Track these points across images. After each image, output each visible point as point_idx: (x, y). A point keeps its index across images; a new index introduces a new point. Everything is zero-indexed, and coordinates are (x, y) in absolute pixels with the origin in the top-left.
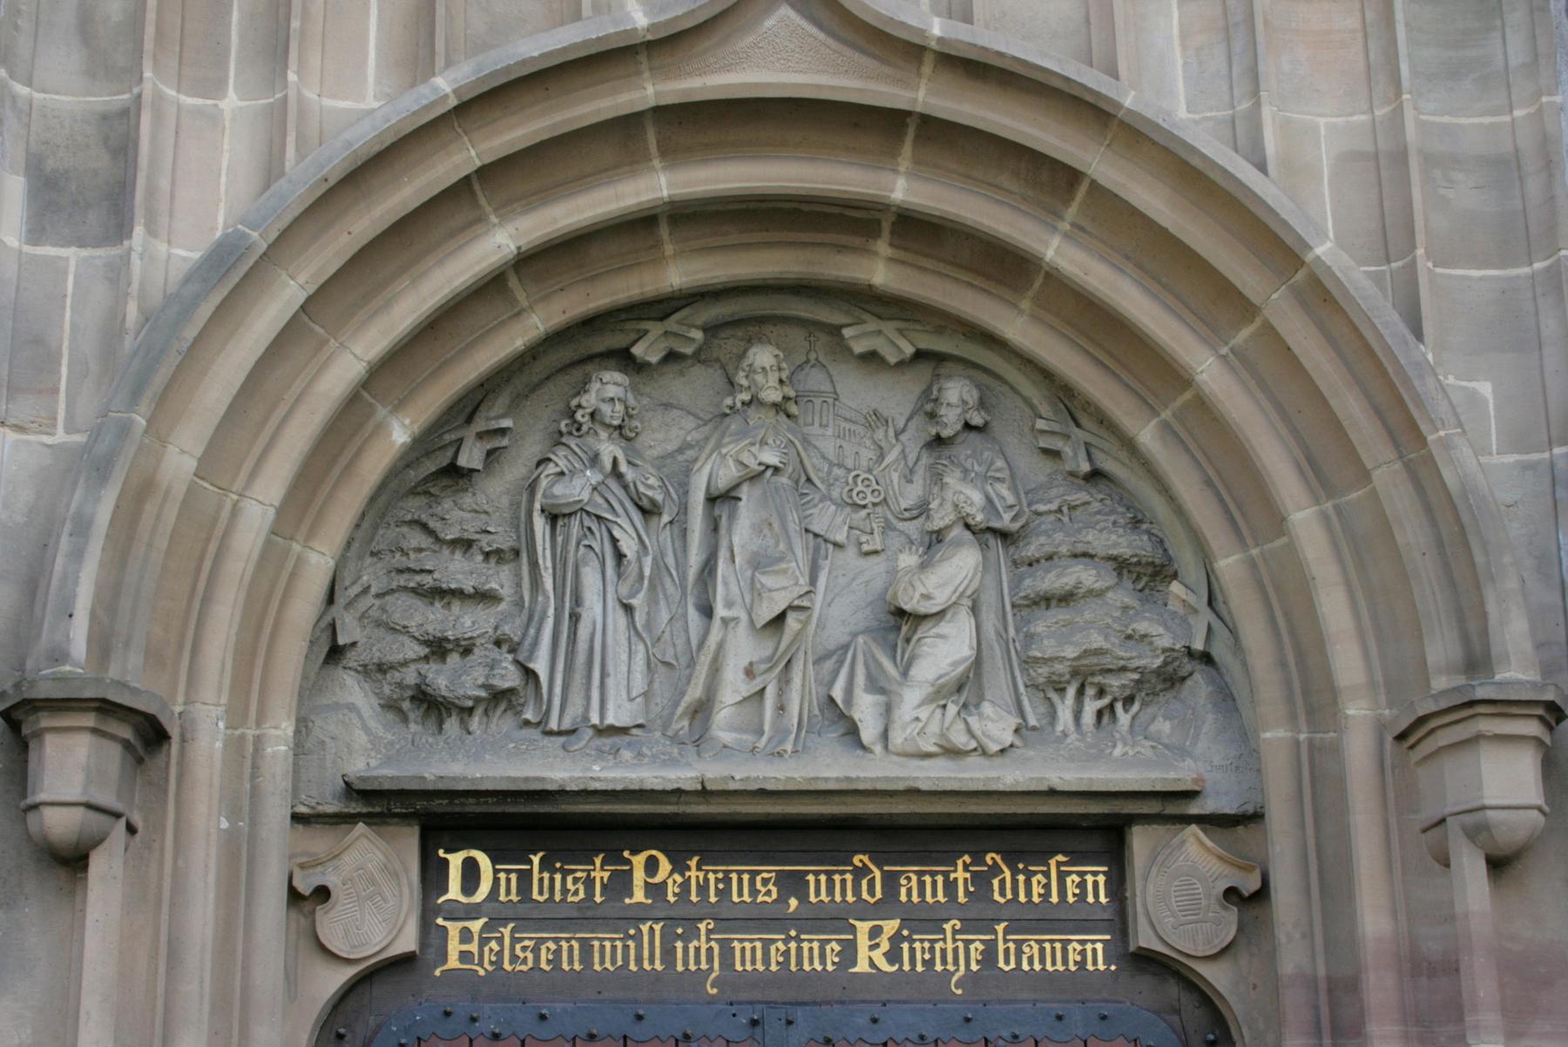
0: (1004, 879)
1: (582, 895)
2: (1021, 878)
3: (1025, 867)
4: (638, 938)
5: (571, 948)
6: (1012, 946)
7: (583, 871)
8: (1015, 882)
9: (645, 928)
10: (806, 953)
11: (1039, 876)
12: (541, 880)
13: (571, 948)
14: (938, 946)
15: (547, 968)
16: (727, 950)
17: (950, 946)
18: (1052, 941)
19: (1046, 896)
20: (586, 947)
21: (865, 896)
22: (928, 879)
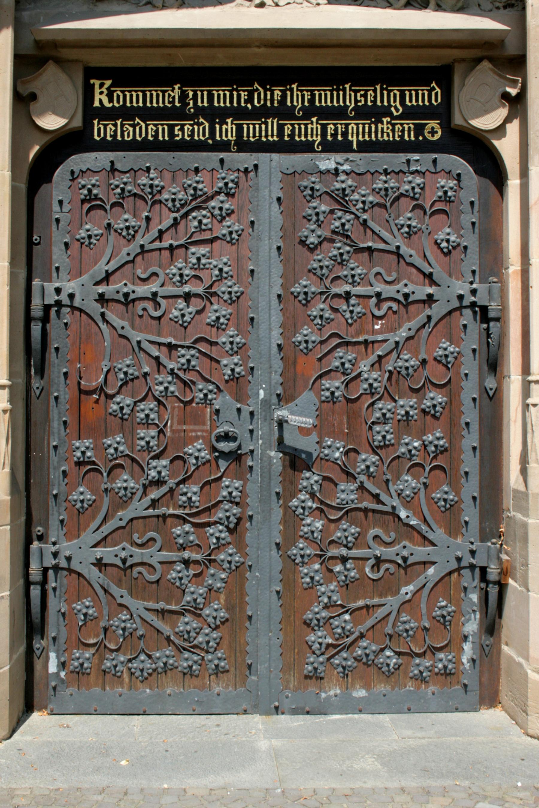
0: (437, 92)
1: (363, 102)
2: (385, 92)
3: (237, 88)
4: (266, 123)
5: (163, 130)
6: (102, 127)
7: (363, 90)
8: (265, 95)
9: (270, 121)
10: (309, 131)
11: (371, 92)
12: (297, 95)
13: (163, 130)
14: (310, 126)
15: (188, 139)
16: (240, 128)
17: (315, 126)
18: (162, 125)
19: (374, 101)
20: (171, 128)
21: (433, 102)
22: (221, 93)
